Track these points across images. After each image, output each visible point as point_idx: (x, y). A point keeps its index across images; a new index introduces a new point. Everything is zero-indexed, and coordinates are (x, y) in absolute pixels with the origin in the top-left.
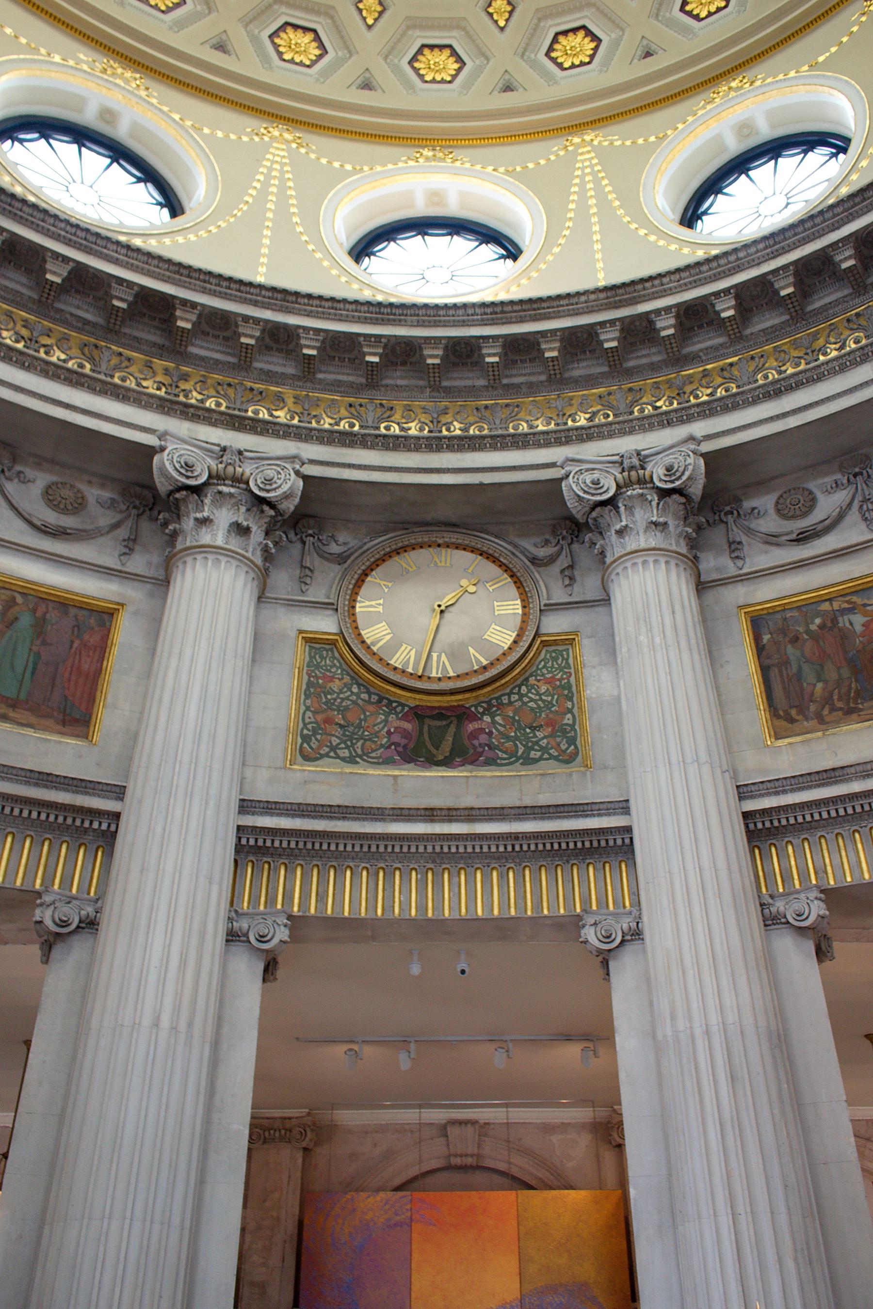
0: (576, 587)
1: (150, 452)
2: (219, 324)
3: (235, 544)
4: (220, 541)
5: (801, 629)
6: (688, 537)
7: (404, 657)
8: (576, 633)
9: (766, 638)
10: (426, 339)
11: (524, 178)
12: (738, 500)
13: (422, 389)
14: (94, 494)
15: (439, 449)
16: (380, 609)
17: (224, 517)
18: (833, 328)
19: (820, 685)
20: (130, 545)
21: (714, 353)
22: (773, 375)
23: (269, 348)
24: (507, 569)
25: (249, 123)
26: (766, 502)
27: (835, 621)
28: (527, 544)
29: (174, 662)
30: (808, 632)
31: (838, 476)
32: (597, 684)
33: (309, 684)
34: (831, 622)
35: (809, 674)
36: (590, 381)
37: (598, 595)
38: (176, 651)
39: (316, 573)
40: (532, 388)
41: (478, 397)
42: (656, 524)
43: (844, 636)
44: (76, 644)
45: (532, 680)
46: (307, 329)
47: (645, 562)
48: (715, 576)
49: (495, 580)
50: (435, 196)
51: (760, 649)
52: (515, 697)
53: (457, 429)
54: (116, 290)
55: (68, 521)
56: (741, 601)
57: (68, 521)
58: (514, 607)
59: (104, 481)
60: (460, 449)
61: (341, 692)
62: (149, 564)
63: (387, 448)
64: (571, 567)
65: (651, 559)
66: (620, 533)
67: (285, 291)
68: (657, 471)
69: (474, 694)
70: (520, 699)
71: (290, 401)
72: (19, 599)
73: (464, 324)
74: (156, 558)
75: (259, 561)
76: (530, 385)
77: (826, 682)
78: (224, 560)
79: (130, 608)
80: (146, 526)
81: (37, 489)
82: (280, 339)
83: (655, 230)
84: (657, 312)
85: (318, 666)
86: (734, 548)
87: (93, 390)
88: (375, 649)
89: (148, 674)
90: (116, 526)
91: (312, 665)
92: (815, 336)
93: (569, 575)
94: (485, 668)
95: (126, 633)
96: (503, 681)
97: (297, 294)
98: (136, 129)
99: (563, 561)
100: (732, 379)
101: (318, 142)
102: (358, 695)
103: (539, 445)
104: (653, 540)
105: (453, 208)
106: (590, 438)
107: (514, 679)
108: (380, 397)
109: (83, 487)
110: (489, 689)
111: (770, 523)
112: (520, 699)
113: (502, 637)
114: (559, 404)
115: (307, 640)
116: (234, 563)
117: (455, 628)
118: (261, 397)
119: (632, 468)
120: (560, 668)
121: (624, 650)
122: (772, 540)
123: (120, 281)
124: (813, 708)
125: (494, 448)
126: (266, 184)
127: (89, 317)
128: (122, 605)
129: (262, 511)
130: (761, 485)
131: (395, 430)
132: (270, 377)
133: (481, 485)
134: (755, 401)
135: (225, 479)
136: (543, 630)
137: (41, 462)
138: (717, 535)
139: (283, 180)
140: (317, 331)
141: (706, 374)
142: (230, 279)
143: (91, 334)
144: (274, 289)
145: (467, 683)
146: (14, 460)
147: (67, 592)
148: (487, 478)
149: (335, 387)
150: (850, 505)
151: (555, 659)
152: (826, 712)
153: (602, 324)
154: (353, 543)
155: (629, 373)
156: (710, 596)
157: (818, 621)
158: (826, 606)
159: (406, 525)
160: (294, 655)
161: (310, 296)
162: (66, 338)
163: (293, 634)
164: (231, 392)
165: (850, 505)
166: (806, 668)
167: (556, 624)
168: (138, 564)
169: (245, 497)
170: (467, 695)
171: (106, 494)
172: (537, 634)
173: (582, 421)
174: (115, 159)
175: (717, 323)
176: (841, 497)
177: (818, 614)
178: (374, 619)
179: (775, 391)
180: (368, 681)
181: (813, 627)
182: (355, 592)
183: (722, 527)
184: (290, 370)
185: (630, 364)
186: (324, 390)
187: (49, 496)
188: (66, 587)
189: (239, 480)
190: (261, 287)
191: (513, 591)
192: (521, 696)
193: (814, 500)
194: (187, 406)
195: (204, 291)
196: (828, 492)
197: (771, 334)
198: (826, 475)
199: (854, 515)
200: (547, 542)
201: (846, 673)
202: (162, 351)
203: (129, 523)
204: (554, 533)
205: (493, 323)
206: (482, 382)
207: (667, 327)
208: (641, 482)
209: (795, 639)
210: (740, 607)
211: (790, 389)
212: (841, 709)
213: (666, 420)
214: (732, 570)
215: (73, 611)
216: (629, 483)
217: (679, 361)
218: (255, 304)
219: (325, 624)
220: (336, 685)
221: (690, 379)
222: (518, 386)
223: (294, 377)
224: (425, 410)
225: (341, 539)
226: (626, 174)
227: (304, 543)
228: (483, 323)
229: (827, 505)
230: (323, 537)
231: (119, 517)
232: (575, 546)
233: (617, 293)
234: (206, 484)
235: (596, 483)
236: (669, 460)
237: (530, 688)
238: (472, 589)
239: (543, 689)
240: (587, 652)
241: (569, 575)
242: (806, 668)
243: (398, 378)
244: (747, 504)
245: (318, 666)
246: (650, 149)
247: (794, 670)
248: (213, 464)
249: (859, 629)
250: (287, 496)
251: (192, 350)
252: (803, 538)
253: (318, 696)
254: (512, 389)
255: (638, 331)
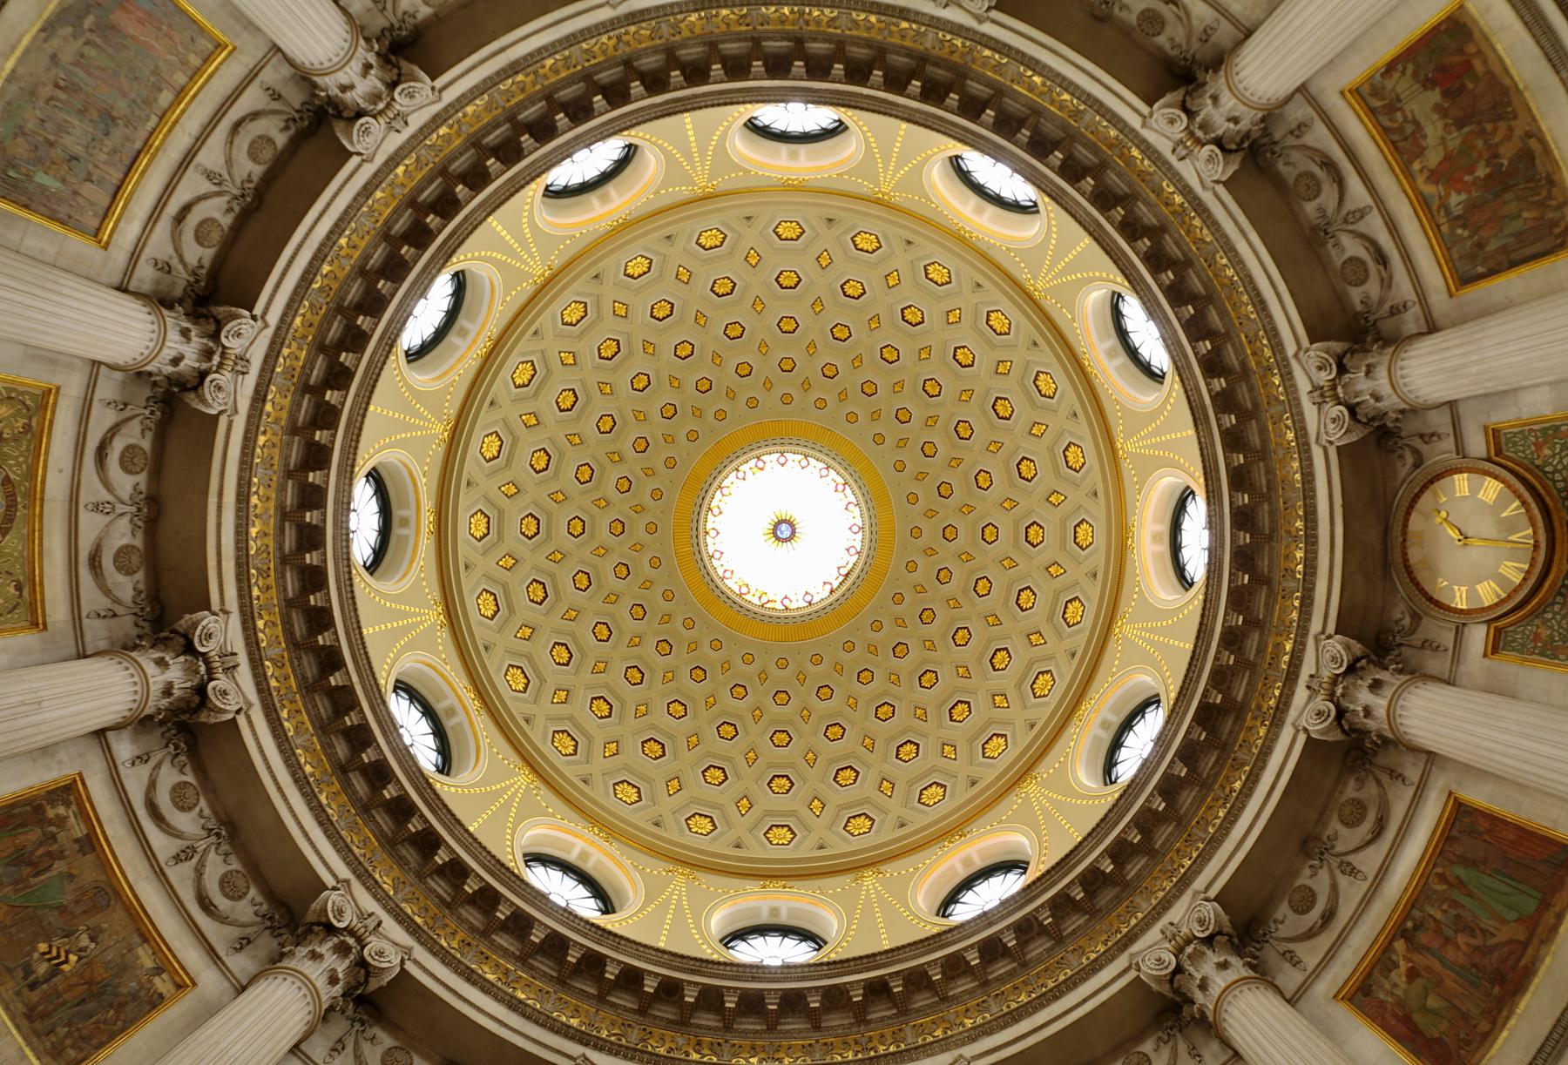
0: (1441, 431)
1: (1310, 742)
2: (1220, 677)
3: (1388, 692)
4: (1384, 703)
5: (1469, 243)
6: (1382, 347)
7: (1513, 571)
8: (1486, 428)
9: (1480, 269)
10: (1232, 542)
11: (1142, 483)
12: (1356, 315)
13: (1271, 548)
14: (1350, 791)
15: (1316, 537)
16: (1464, 589)
17: (1364, 697)
18: (1216, 275)
19: (1525, 215)
20: (1397, 776)
21: (1239, 350)
22: (1250, 308)
23: (1240, 648)
24: (1424, 488)
25: (1111, 645)
26: (1355, 294)
27: (1458, 218)
28: (1403, 472)
29: (1497, 757)
30: (1471, 237)
31: (1329, 246)
32: (1538, 405)
33: (1542, 654)
34: (1461, 220)
35: (1517, 225)
36: (1263, 432)
37: (1446, 410)
38: (1486, 754)
39: (1430, 637)
40: (1269, 472)
41: (1277, 509)
42: (1368, 373)
43: (1472, 207)
44: (1486, 837)
45: (1537, 462)
46: (1225, 621)
47: (1402, 377)
48: (1423, 322)
49: (1436, 495)
50: (1156, 538)
51: (1492, 273)
52: (1558, 477)
53: (1299, 524)
54: (1194, 736)
55: (1371, 816)
56: (1445, 296)
57: (1371, 816)
58: (1461, 483)
59: (1340, 782)
60: (1315, 521)
61: (1551, 628)
62: (1414, 764)
63: (1315, 574)
64: (1422, 436)
65: (1399, 373)
66: (1378, 399)
67: (1199, 631)
68: (1324, 377)
69: (1553, 512)
70: (1559, 471)
71: (1279, 639)
72: (1439, 870)
73: (1222, 517)
74: (1409, 759)
75: (1404, 678)
76: (1267, 473)
77: (1521, 210)
78: (1401, 702)
79: (1454, 788)
80: (1381, 760)
81: (1343, 831)
82: (1231, 639)
83: (1166, 401)
84: (1210, 391)
85: (1523, 645)
86: (1395, 311)
87: (1263, 768)
88: (1504, 595)
89: (1523, 787)
90: (1379, 782)
91: (1522, 649)
92: (1222, 285)
93: (1429, 437)
94: (1524, 503)
95: (1478, 795)
96: (1539, 487)
97: (1201, 624)
98: (1115, 710)
99: (1417, 443)
100: (1256, 335)
101: (1122, 607)
102: (1556, 613)
103: (1311, 465)
104: (1382, 372)
105: (1164, 528)
106: (1304, 428)
107: (1537, 477)
108: (1277, 577)
109: (1344, 798)
110: (1548, 500)
111: (1373, 288)
112: (1559, 471)
113: (1491, 489)
114: (1281, 453)
115: (1495, 650)
116: (1405, 695)
117: (1482, 526)
118: (1276, 657)
119: (1322, 395)
120: (1525, 438)
121: (1489, 384)
122: (1387, 283)
123: (1188, 732)
124: (1550, 215)
125: (1314, 497)
126: (1144, 639)
127: (1213, 759)
128: (1450, 793)
129: (1362, 668)
130: (1341, 300)
131: (1300, 568)
132: (1261, 651)
133: (1343, 506)
134: (1269, 316)
135: (1335, 690)
136: (1484, 455)
137: (1322, 820)
138: (1387, 326)
139: (1142, 629)
140: (1226, 614)
141: (1254, 353)
142: (1190, 664)
143: (1225, 761)
144: (1197, 638)
145: (1539, 518)
146: (1318, 839)
147: (1434, 832)
148: (1338, 501)
149: (1269, 607)
150: (1351, 232)
151: (1515, 444)
152: (1553, 203)
153: (1219, 426)
154: (1402, 607)
155: (1256, 406)
156: (1440, 322)
157: (1459, 231)
158: (1445, 229)
159: (1386, 564)
160: (1509, 667)
161: (1203, 616)
162: (1227, 778)
163: (1487, 662)
164: (1271, 679)
165: (1351, 232)
166: (1507, 231)
167: (1477, 445)
168: (1413, 773)
169: (1350, 679)
170: (1555, 518)
171: (1352, 783)
172: (1489, 460)
173: (1290, 435)
174: (1131, 728)
175: (1217, 351)
176: (1346, 240)
177: (1453, 233)
178: (1472, 594)
179: (1261, 304)
180: (1539, 604)
181: (1466, 233)
182: (1448, 609)
183: (1379, 323)
184: (1256, 636)
185: (1249, 405)
186: (1272, 615)
187: (1352, 822)
188: (1429, 833)
189: (1335, 681)
190: (1195, 646)
191: (1444, 482)
192: (1556, 471)
193: (1351, 259)
194: (1277, 708)
195: (1198, 682)
196: (1343, 250)
197: (1223, 314)
198: (1329, 255)
199: (1361, 227)
200: (1401, 457)
201: (1509, 196)
202: (1240, 718)
203: (1377, 772)
204: (1393, 452)
205: (1221, 498)
206: (1266, 506)
207: (1220, 384)
208: (1334, 388)
209: (1480, 246)
210: (1451, 296)
211: (1258, 294)
212: (1549, 191)
213: (1287, 376)
214: (1417, 309)
215: (1455, 833)
216: (1336, 397)
217: (1245, 372)
218: (1207, 651)
219: (1478, 636)
220: (1545, 632)
221: (1258, 363)
222: (1269, 482)
223: (1261, 634)
224: (1287, 546)
225: (1399, 616)
226: (512, 276)
227: (1401, 645)
228: (1221, 505)
229: (1353, 248)
230: (1396, 629)
231: (1371, 778)
232: (1403, 434)
233: (1199, 419)
234: (1338, 706)
235: (1334, 421)
236: (1314, 370)
237: (1546, 463)
238: (1444, 514)
239: (1547, 452)
240: (1503, 416)
241: (1429, 437)
242: (1507, 231)
243: (1263, 564)
244: (1359, 308)
245: (1523, 645)
246: (1124, 409)
247: (1511, 239)
248: (1320, 697)
249: (1463, 197)
250: (1347, 648)
251: (1239, 698)
252: (1382, 259)
253: (1557, 648)
254: (1271, 485)
255: (1224, 402)
